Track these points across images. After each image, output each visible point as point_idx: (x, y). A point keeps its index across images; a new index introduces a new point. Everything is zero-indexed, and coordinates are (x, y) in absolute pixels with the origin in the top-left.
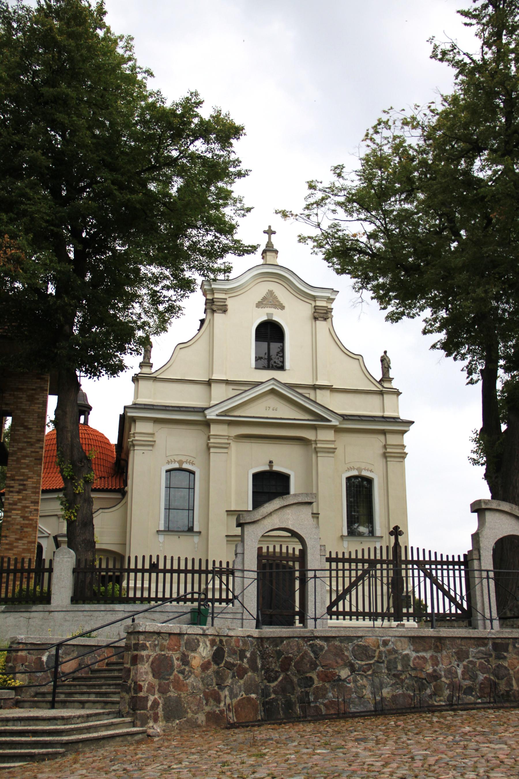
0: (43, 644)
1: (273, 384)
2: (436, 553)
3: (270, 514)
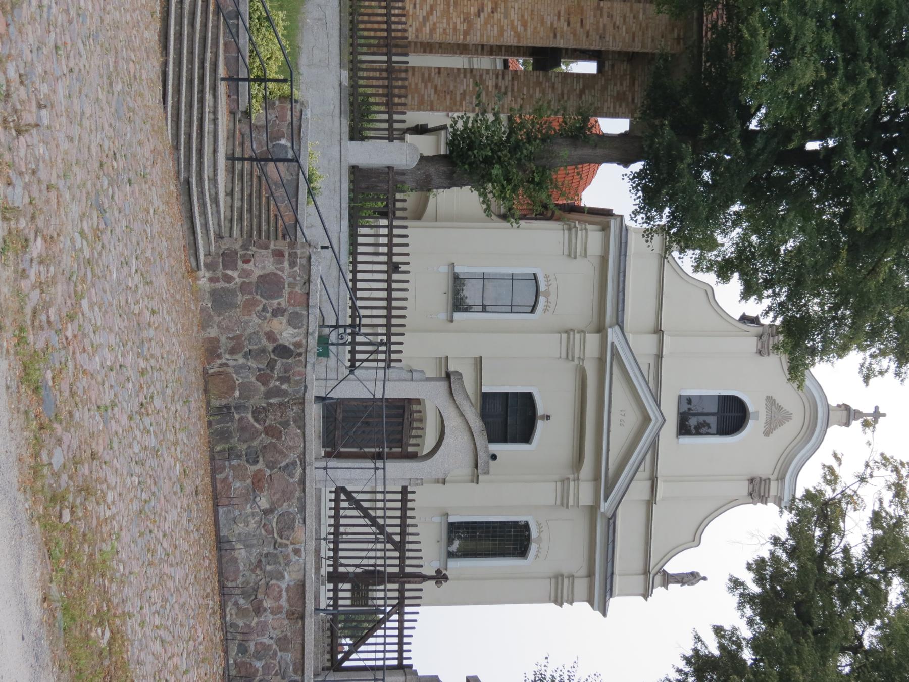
0: (300, 139)
1: (657, 420)
2: (413, 628)
3: (462, 415)
